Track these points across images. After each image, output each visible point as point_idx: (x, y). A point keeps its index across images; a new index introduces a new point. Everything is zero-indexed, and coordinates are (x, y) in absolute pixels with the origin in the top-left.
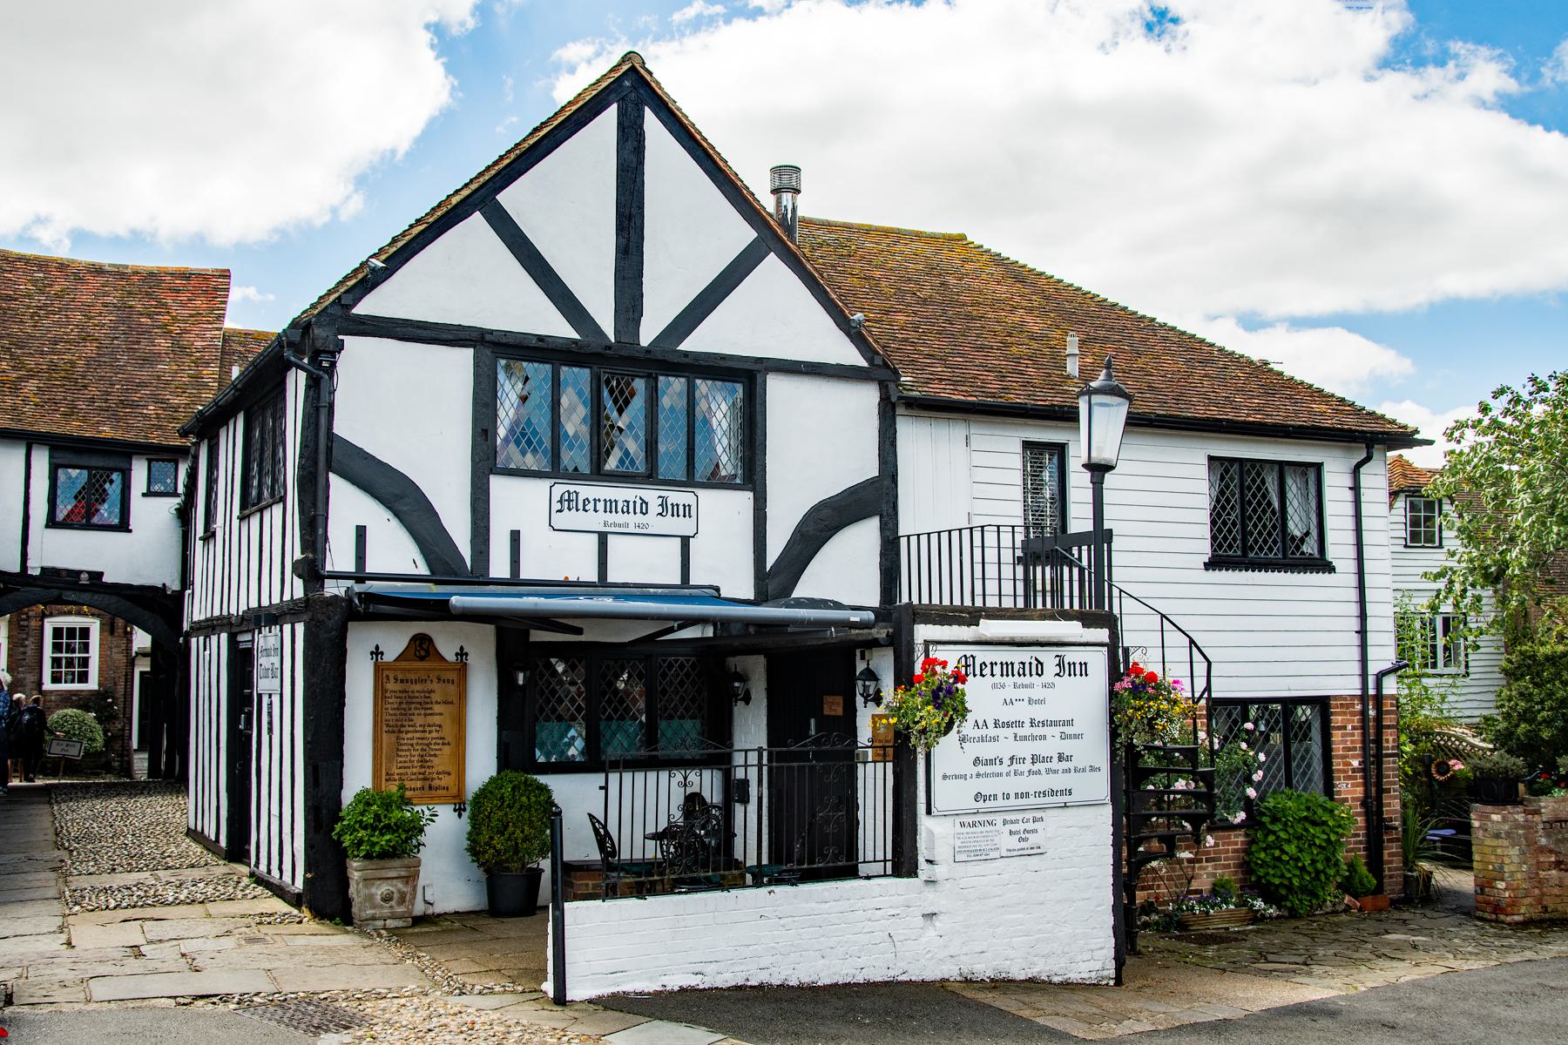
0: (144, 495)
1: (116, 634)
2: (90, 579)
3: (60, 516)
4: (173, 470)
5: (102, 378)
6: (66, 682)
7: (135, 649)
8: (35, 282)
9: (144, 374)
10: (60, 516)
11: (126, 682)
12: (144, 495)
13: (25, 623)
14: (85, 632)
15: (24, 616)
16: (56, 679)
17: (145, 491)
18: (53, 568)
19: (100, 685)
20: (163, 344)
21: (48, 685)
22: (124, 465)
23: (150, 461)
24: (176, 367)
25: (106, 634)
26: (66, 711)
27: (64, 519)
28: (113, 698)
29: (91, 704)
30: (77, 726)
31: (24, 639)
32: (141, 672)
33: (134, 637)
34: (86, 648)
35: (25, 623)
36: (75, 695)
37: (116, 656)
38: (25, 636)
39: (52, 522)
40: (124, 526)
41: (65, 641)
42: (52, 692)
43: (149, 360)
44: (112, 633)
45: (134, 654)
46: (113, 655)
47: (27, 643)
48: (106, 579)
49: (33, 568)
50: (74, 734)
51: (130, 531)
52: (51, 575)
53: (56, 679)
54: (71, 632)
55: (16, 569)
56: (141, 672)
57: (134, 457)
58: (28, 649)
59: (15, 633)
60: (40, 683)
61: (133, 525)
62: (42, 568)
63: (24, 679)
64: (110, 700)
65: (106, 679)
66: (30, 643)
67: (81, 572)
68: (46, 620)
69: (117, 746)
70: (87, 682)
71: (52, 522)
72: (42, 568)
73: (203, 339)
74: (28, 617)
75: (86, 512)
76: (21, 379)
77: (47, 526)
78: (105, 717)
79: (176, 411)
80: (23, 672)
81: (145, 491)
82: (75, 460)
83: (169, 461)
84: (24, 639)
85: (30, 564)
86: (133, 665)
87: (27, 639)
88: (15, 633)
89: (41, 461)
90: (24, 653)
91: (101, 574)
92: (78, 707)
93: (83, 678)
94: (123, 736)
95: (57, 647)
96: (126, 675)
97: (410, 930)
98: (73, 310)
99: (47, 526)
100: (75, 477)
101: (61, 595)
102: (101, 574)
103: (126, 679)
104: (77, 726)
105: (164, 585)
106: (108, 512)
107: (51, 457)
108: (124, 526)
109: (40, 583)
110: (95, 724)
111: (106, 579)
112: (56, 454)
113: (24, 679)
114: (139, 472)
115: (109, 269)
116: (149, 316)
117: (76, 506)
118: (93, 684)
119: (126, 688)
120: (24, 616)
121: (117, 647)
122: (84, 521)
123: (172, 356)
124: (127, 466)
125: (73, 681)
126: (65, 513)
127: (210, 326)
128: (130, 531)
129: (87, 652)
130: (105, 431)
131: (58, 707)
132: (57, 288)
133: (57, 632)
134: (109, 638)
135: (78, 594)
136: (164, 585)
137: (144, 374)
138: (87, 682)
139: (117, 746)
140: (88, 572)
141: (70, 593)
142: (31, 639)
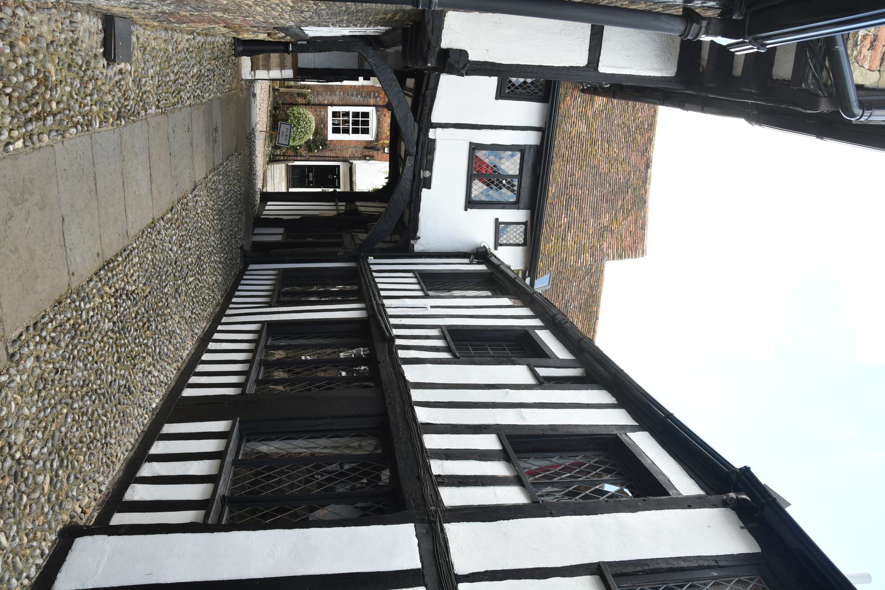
0: (497, 220)
1: (365, 150)
2: (425, 178)
3: (480, 154)
4: (517, 242)
5: (586, 179)
6: (333, 120)
7: (354, 162)
8: (642, 123)
9: (587, 210)
10: (480, 154)
11: (333, 157)
12: (497, 220)
13: (372, 96)
14: (366, 131)
15: (376, 95)
16: (335, 114)
17: (500, 221)
18: (434, 149)
19: (331, 141)
20: (605, 220)
21: (331, 110)
22: (522, 204)
23: (525, 224)
24: (591, 233)
25: (365, 144)
26: (314, 122)
27: (477, 157)
28: (323, 149)
29: (318, 136)
30: (303, 130)
31: (361, 95)
32: (338, 166)
33: (363, 161)
34: (355, 131)
35: (372, 96)
36: (324, 126)
37: (350, 150)
38: (363, 95)
39: (474, 148)
40: (471, 203)
41: (360, 127)
42: (327, 112)
43: (596, 214)
44: (365, 148)
45: (351, 161)
46: (351, 149)
47: (359, 96)
48: (424, 191)
49: (435, 133)
50: (298, 128)
51: (466, 210)
52: (426, 150)
53: (335, 114)
54: (366, 123)
55: (435, 118)
56: (338, 166)
57: (529, 211)
58: (355, 97)
59: (366, 90)
60: (332, 105)
61: (472, 212)
62: (434, 141)
63: (336, 96)
64: (321, 147)
65: (335, 145)
66: (359, 99)
67: (431, 170)
68: (374, 108)
69: (291, 152)
70: (333, 132)
71: (474, 148)
72: (434, 141)
73: (609, 248)
74: (376, 97)
75: (482, 174)
76: (587, 119)
77: (471, 143)
78: (309, 146)
79: (562, 239)
80: (340, 95)
81: (500, 221)
82: (528, 165)
83: (525, 239)
84: (361, 95)
85: (439, 130)
86: (345, 160)
87: (362, 96)
88: (366, 90)
89: (530, 139)
90: (352, 95)
91: (429, 187)
92: (316, 129)
93: (336, 131)
94: (297, 156)
95: (356, 115)
96: (337, 157)
97: (292, 83)
98: (627, 151)
99: (471, 143)
100: (510, 166)
101: (410, 155)
102: (429, 187)
103: (335, 157)
104: (303, 130)
105: (419, 238)
106: (478, 188)
107: (530, 146)
108: (471, 203)
109: (422, 138)
110: (305, 140)
111: (424, 191)
112: (532, 150)
113: (336, 96)
114: (519, 215)
115: (649, 173)
116: (622, 205)
117: (488, 166)
118: (331, 136)
119: (328, 157)
120: (376, 95)
121: (356, 152)
122: (475, 173)
123: (598, 228)
124: (521, 206)
125: (333, 124)
126: (483, 158)
127: (615, 251)
128: (466, 210)
129: (353, 133)
130: (552, 189)
131: (316, 116)
132: (639, 138)
133: (366, 115)
134: (362, 146)
135: (412, 169)
136: (419, 238)
137: (587, 210)
138: (333, 132)
139: (291, 152)
140: (430, 177)
141: (413, 162)
142: (362, 99)
